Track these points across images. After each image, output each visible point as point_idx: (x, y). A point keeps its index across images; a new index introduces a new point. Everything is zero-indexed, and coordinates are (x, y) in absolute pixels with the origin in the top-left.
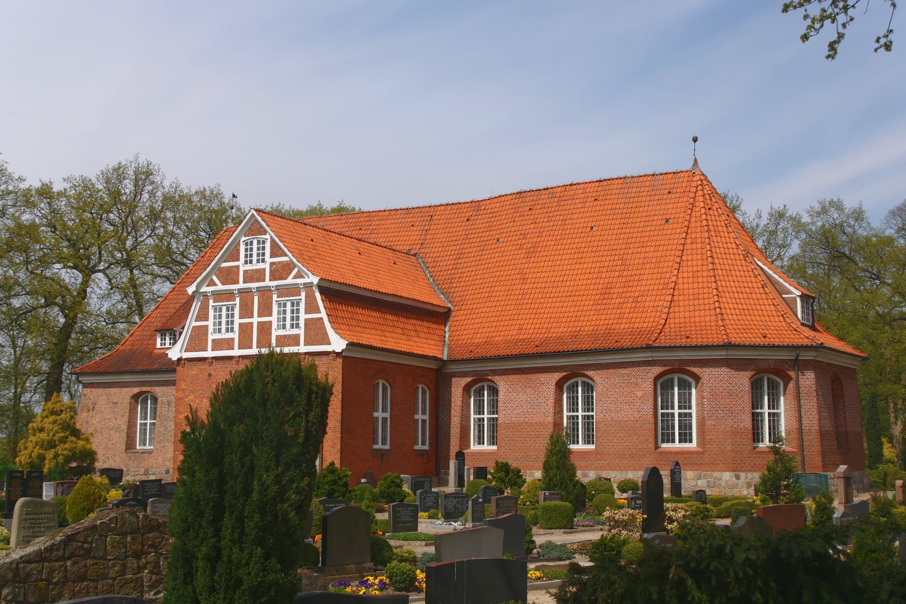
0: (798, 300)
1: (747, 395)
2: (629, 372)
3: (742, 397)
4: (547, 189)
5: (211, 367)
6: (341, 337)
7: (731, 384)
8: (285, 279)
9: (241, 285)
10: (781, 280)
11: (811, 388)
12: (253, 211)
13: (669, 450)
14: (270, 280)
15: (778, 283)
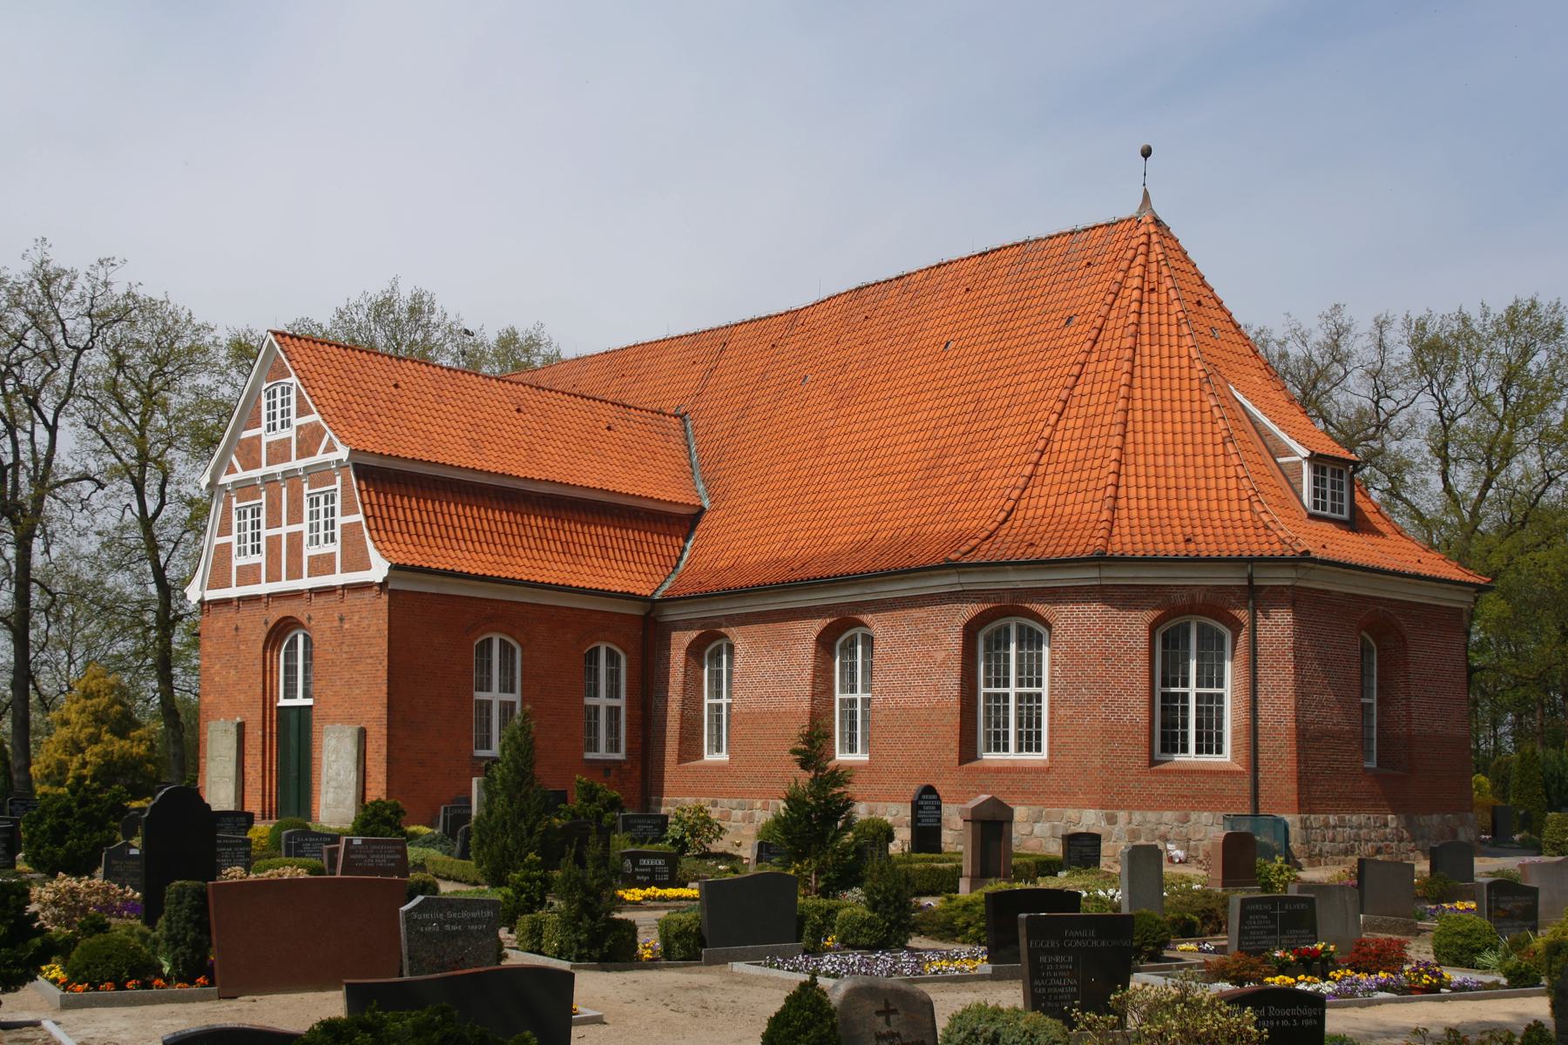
0: (1305, 466)
2: (925, 615)
3: (1131, 661)
4: (902, 277)
5: (238, 615)
6: (382, 555)
7: (1107, 635)
8: (314, 454)
9: (265, 470)
10: (1275, 428)
11: (1283, 643)
12: (271, 336)
14: (298, 458)
15: (1270, 434)
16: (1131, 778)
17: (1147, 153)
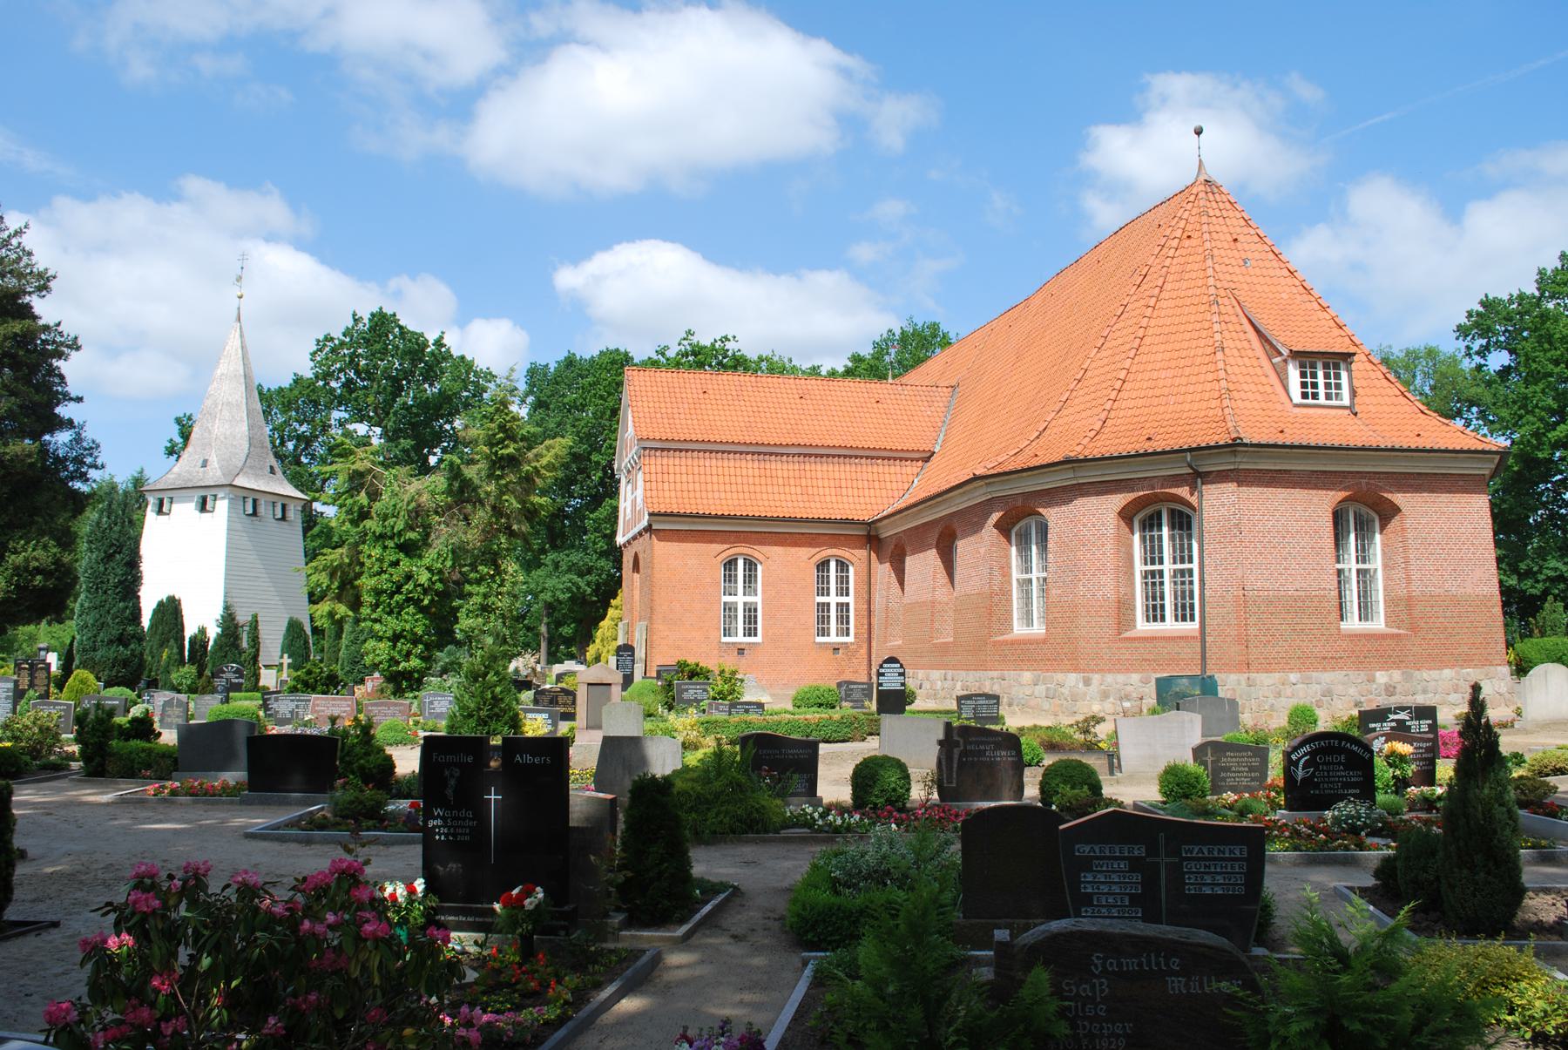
1: (1112, 541)
3: (1103, 545)
13: (1022, 638)
16: (1104, 646)
17: (1199, 132)
